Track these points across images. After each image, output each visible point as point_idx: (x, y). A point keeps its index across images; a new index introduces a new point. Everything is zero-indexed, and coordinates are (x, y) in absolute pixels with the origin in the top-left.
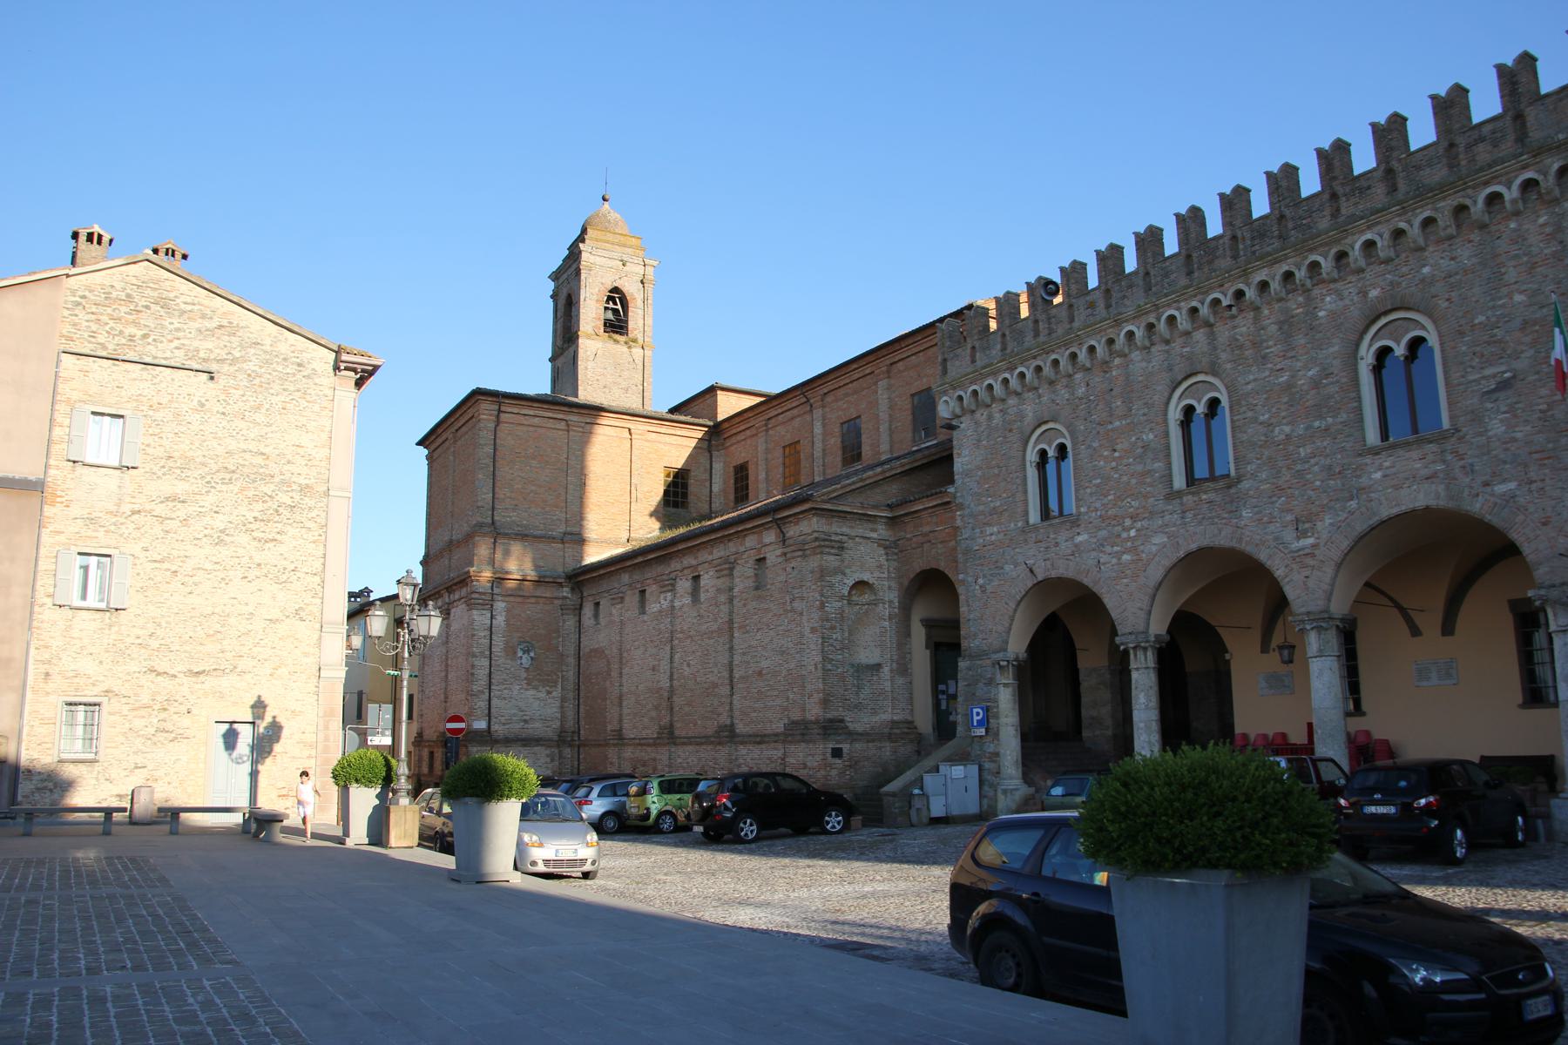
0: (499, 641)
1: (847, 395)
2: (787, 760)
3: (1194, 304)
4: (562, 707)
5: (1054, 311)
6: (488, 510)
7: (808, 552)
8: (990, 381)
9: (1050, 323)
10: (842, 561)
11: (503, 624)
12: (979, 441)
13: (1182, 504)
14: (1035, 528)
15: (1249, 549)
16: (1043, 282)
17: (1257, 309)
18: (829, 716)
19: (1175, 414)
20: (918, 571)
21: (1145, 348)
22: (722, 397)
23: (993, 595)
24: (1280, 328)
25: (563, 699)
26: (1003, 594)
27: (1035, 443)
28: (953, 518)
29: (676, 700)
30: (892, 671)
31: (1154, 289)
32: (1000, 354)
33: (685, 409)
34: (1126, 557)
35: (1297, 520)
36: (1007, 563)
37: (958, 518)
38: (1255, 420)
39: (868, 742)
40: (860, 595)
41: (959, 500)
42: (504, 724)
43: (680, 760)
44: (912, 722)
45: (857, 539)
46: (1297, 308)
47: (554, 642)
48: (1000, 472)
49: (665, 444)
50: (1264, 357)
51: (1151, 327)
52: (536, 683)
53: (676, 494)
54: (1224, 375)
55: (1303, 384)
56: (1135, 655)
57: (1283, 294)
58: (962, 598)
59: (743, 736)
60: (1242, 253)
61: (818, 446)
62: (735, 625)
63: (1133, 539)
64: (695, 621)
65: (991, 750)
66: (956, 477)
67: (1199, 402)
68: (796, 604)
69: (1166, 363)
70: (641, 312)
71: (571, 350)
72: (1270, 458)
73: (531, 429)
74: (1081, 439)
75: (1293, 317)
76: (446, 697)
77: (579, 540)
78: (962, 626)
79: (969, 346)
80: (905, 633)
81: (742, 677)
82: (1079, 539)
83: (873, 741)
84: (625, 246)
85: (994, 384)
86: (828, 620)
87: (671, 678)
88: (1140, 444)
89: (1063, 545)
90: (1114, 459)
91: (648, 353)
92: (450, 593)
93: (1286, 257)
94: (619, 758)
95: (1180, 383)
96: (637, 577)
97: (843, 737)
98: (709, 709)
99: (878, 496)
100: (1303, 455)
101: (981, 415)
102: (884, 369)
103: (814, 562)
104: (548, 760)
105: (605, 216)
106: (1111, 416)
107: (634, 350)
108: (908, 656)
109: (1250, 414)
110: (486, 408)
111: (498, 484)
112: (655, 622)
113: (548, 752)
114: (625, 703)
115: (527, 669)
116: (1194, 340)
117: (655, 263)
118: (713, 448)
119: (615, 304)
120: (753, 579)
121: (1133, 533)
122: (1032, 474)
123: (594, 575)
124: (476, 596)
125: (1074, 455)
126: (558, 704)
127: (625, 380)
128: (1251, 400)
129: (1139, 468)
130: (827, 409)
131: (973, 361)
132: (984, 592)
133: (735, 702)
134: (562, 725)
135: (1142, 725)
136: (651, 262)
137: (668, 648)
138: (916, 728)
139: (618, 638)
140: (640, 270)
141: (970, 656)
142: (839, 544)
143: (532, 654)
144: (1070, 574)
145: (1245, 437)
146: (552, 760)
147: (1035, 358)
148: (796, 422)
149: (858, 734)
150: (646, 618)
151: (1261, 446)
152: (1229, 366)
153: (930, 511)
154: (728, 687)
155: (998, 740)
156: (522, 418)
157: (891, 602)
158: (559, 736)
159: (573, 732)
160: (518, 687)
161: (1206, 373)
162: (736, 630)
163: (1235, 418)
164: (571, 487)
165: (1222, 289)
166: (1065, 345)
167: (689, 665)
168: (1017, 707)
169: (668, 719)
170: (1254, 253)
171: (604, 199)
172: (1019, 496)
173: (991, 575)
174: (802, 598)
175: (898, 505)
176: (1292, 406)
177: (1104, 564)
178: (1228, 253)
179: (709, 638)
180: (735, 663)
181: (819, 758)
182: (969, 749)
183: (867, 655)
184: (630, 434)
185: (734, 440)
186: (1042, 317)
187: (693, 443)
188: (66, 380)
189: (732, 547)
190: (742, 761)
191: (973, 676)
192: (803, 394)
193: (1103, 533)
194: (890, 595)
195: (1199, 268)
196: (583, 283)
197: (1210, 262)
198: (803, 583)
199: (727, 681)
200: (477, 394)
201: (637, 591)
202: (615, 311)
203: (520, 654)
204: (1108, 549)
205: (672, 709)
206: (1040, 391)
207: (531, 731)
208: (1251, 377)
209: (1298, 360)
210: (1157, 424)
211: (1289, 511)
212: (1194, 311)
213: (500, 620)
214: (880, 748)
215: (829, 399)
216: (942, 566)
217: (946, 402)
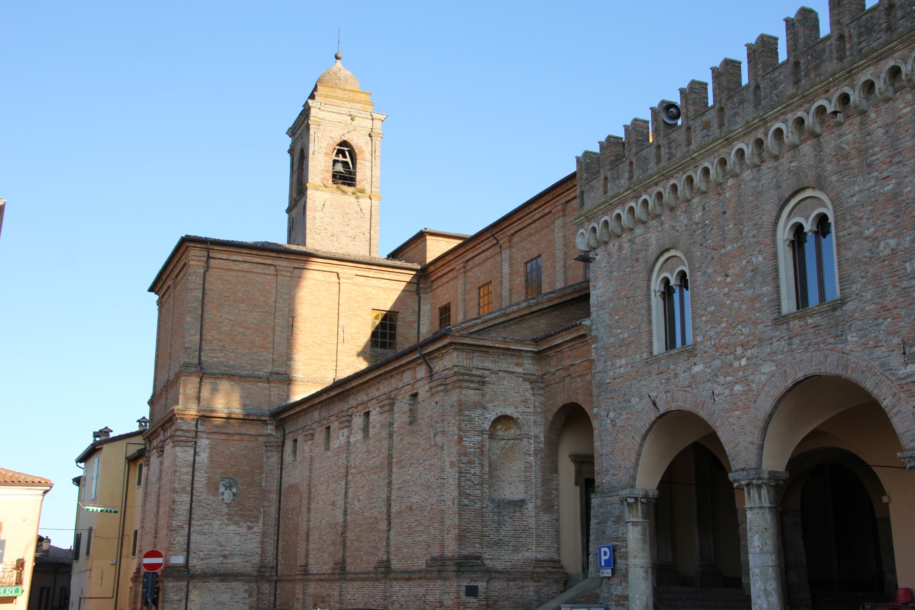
0: (201, 479)
1: (530, 235)
2: (427, 597)
3: (800, 114)
4: (262, 542)
6: (195, 351)
7: (449, 387)
9: (670, 148)
10: (483, 395)
11: (206, 460)
12: (611, 272)
13: (789, 329)
14: (658, 359)
15: (855, 377)
16: (665, 105)
17: (863, 113)
18: (464, 552)
19: (784, 233)
20: (561, 405)
21: (755, 166)
22: (430, 241)
23: (621, 429)
24: (887, 132)
25: (264, 535)
26: (630, 428)
27: (659, 272)
28: (589, 351)
29: (350, 535)
30: (536, 507)
31: (763, 103)
32: (627, 182)
33: (400, 254)
34: (738, 388)
35: (904, 342)
36: (633, 396)
37: (593, 351)
38: (860, 235)
39: (508, 580)
40: (507, 430)
41: (594, 333)
42: (202, 559)
43: (349, 597)
44: (559, 561)
46: (905, 108)
47: (257, 478)
48: (628, 302)
50: (869, 166)
51: (759, 143)
52: (237, 518)
53: (384, 335)
54: (830, 189)
55: (910, 191)
56: (749, 494)
57: (890, 93)
58: (596, 432)
59: (397, 572)
60: (848, 53)
61: (506, 285)
62: (394, 460)
64: (365, 456)
65: (618, 593)
66: (592, 310)
67: (807, 219)
68: (439, 439)
69: (775, 180)
70: (369, 164)
71: (302, 201)
72: (875, 276)
73: (240, 274)
74: (697, 265)
75: (900, 117)
76: (156, 533)
77: (287, 380)
78: (595, 461)
79: (602, 177)
80: (551, 467)
82: (696, 369)
83: (515, 580)
85: (622, 214)
86: (465, 455)
87: (345, 513)
89: (682, 376)
90: (726, 285)
91: (375, 203)
92: (164, 431)
93: (892, 51)
94: (304, 593)
95: (788, 201)
96: (325, 414)
97: (479, 574)
98: (373, 544)
99: (525, 331)
100: (909, 269)
101: (613, 247)
102: (560, 207)
103: (454, 397)
104: (246, 595)
105: (336, 74)
106: (724, 239)
107: (361, 200)
108: (555, 492)
109: (855, 229)
110: (195, 257)
111: (206, 326)
112: (336, 458)
113: (246, 587)
114: (311, 538)
115: (229, 505)
116: (802, 154)
117: (383, 117)
118: (422, 291)
119: (345, 156)
120: (408, 414)
121: (744, 362)
122: (657, 303)
123: (292, 412)
124: (180, 433)
126: (258, 539)
127: (352, 229)
128: (856, 213)
129: (749, 293)
130: (514, 250)
131: (605, 192)
132: (614, 426)
133: (392, 537)
134: (262, 561)
135: (757, 571)
136: (379, 116)
137: (343, 483)
138: (562, 567)
139: (308, 474)
140: (369, 124)
141: (603, 492)
142: (479, 379)
143: (234, 490)
144: (688, 407)
145: (849, 254)
146: (250, 596)
147: (656, 184)
148: (489, 264)
149: (496, 572)
150: (329, 454)
151: (866, 263)
152: (834, 178)
153: (570, 344)
154: (386, 522)
155: (627, 582)
156: (231, 264)
157: (536, 437)
158: (259, 572)
159: (272, 568)
160: (219, 522)
161: (814, 188)
162: (394, 465)
163: (840, 234)
164: (278, 328)
165: (827, 95)
166: (682, 169)
167: (359, 500)
169: (341, 554)
170: (860, 50)
171: (337, 58)
172: (644, 327)
173: (620, 408)
174: (444, 433)
175: (541, 340)
176: (898, 216)
177: (718, 395)
178: (835, 55)
179: (375, 473)
180: (393, 497)
181: (453, 596)
182: (598, 590)
183: (512, 490)
184: (339, 278)
186: (663, 142)
187: (402, 286)
189: (394, 383)
190: (395, 598)
191: (603, 513)
192: (493, 235)
193: (718, 363)
195: (806, 75)
196: (311, 138)
197: (817, 67)
198: (444, 418)
199: (385, 516)
200: (186, 242)
201: (324, 428)
202: (345, 164)
203: (222, 489)
204: (721, 379)
205: (345, 544)
207: (230, 566)
208: (857, 189)
209: (904, 165)
210: (766, 245)
211: (896, 333)
212: (800, 121)
213: (203, 457)
214: (523, 587)
215: (516, 239)
216: (581, 400)
217: (582, 234)
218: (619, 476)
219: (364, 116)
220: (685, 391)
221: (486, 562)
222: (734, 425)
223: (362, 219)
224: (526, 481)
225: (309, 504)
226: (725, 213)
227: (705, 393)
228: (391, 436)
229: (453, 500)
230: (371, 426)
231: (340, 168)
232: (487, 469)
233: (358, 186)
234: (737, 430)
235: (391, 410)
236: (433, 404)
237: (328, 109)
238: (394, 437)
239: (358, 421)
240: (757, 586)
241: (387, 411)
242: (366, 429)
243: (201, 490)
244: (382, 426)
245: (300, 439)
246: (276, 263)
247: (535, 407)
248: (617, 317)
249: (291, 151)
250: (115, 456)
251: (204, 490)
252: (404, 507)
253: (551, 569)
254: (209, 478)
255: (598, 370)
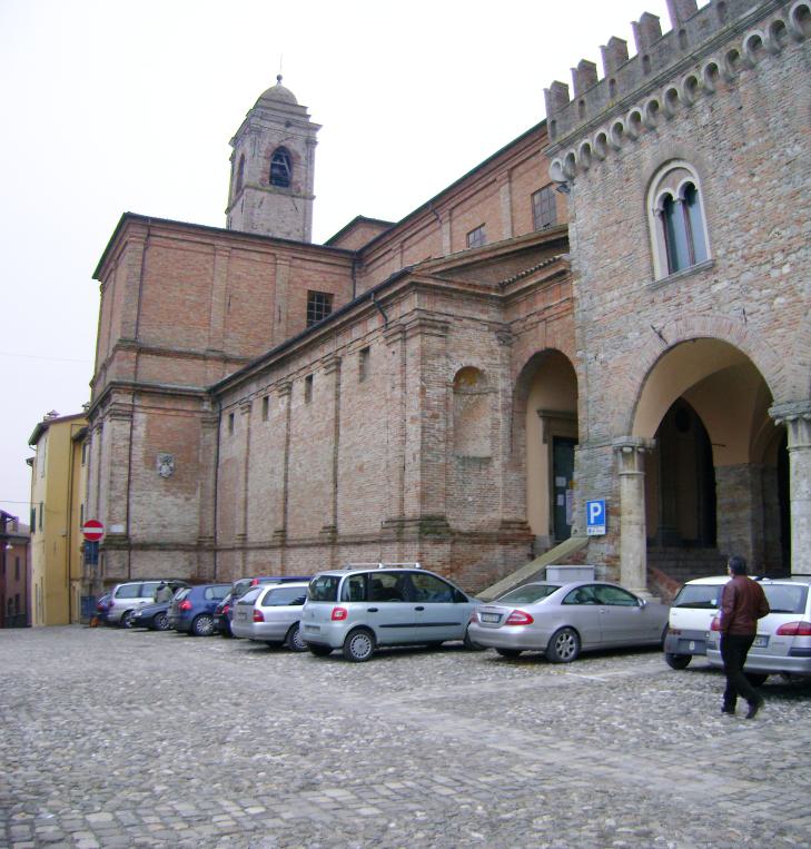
1: (472, 206)
4: (201, 513)
5: (665, 42)
7: (409, 334)
8: (601, 130)
11: (143, 435)
25: (202, 506)
30: (504, 465)
37: (575, 288)
44: (526, 523)
45: (465, 320)
52: (174, 490)
56: (796, 431)
58: (580, 379)
59: (345, 537)
63: (787, 278)
81: (345, 474)
85: (606, 134)
86: (428, 408)
87: (286, 480)
88: (785, 160)
96: (263, 384)
104: (187, 563)
106: (744, 135)
108: (522, 449)
113: (187, 555)
119: (282, 161)
120: (358, 372)
121: (786, 269)
122: (655, 223)
125: (704, 191)
126: (196, 510)
129: (787, 189)
134: (201, 532)
135: (803, 520)
138: (529, 529)
143: (172, 465)
144: (708, 333)
146: (191, 564)
149: (460, 533)
150: (268, 424)
153: (545, 284)
154: (332, 485)
156: (170, 242)
157: (504, 391)
168: (643, 502)
182: (584, 551)
183: (479, 446)
185: (375, 265)
189: (341, 341)
194: (503, 383)
204: (755, 294)
206: (658, 130)
213: (140, 431)
215: (456, 213)
217: (557, 163)
218: (611, 424)
220: (704, 315)
221: (451, 523)
222: (776, 345)
224: (493, 437)
225: (247, 473)
226: (741, 108)
227: (733, 313)
228: (337, 396)
229: (414, 455)
230: (314, 390)
231: (276, 171)
232: (451, 425)
234: (781, 351)
235: (338, 371)
236: (390, 355)
238: (341, 398)
239: (299, 387)
240: (803, 537)
241: (332, 372)
242: (308, 396)
243: (139, 463)
244: (327, 387)
245: (237, 413)
246: (215, 242)
247: (502, 358)
248: (605, 247)
249: (232, 159)
250: (60, 437)
251: (142, 464)
252: (353, 468)
253: (517, 531)
254: (146, 453)
255: (581, 308)
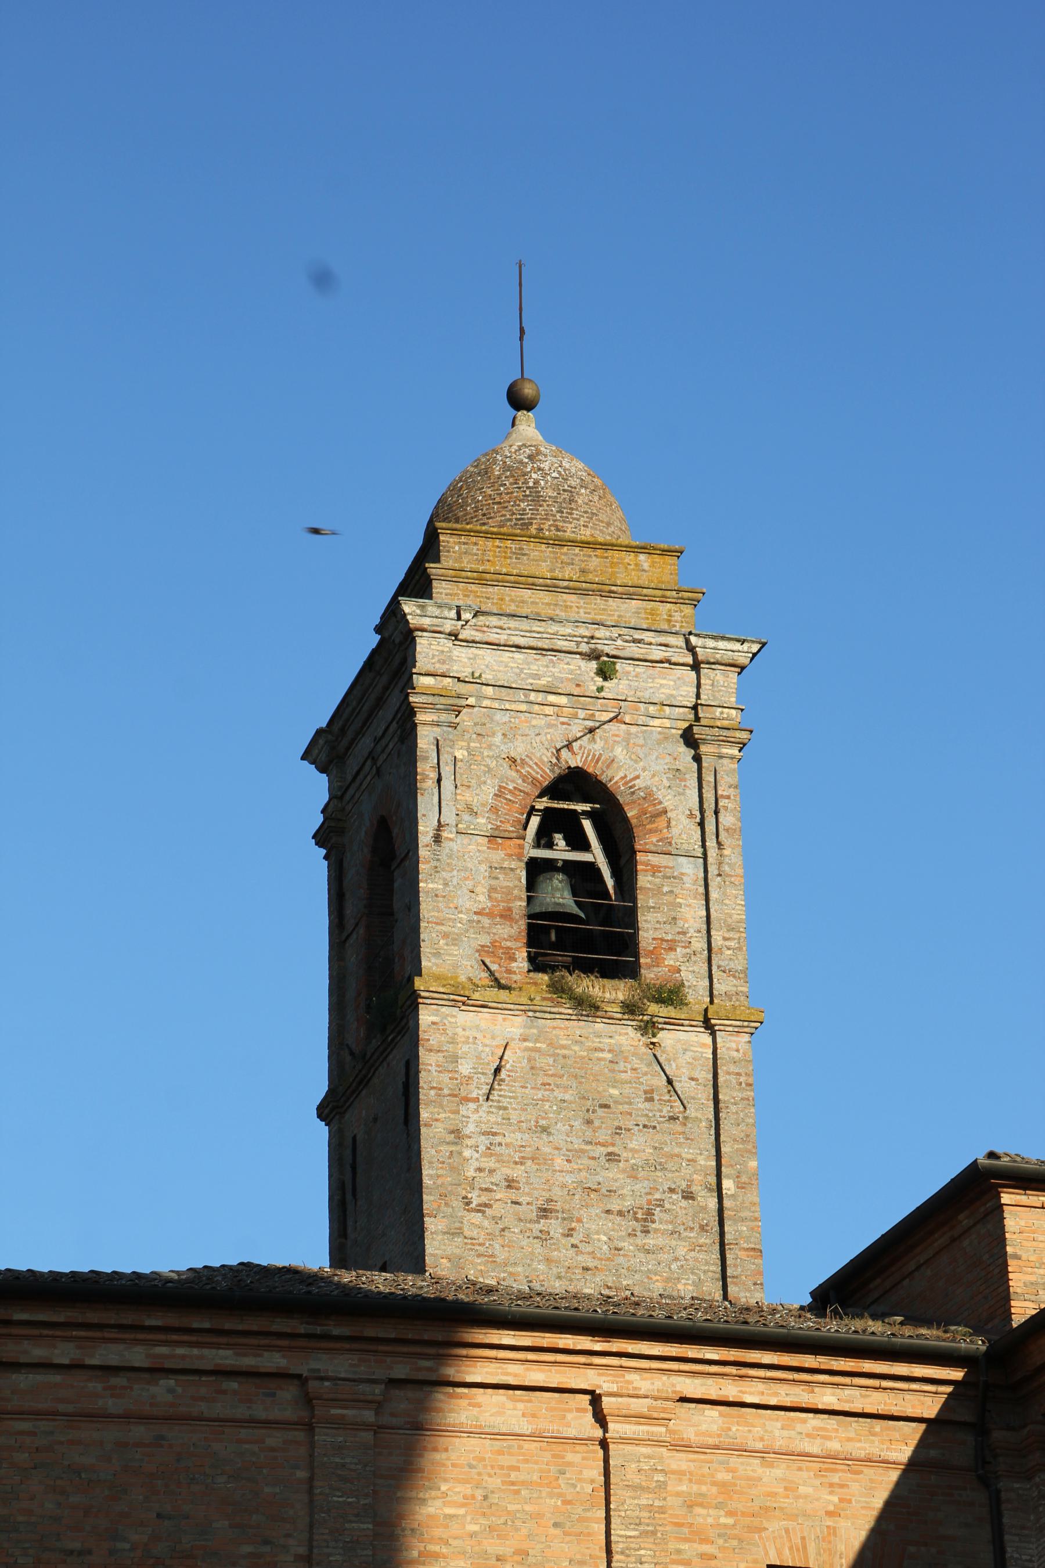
49: (765, 1454)
70: (691, 870)
73: (139, 1432)
84: (606, 591)
107: (666, 1038)
117: (741, 652)
119: (579, 842)
184: (601, 1419)
188: (487, 1084)
196: (425, 768)
219: (658, 654)
223: (677, 1127)
233: (649, 974)
237: (493, 637)
